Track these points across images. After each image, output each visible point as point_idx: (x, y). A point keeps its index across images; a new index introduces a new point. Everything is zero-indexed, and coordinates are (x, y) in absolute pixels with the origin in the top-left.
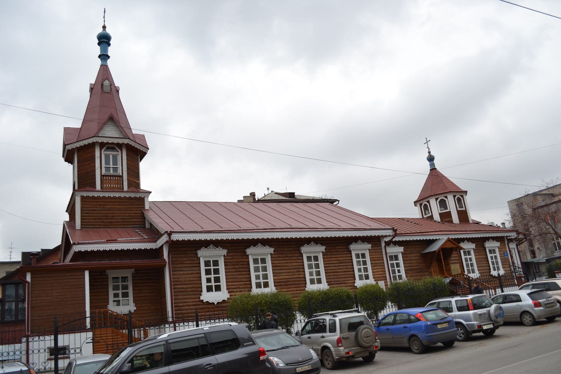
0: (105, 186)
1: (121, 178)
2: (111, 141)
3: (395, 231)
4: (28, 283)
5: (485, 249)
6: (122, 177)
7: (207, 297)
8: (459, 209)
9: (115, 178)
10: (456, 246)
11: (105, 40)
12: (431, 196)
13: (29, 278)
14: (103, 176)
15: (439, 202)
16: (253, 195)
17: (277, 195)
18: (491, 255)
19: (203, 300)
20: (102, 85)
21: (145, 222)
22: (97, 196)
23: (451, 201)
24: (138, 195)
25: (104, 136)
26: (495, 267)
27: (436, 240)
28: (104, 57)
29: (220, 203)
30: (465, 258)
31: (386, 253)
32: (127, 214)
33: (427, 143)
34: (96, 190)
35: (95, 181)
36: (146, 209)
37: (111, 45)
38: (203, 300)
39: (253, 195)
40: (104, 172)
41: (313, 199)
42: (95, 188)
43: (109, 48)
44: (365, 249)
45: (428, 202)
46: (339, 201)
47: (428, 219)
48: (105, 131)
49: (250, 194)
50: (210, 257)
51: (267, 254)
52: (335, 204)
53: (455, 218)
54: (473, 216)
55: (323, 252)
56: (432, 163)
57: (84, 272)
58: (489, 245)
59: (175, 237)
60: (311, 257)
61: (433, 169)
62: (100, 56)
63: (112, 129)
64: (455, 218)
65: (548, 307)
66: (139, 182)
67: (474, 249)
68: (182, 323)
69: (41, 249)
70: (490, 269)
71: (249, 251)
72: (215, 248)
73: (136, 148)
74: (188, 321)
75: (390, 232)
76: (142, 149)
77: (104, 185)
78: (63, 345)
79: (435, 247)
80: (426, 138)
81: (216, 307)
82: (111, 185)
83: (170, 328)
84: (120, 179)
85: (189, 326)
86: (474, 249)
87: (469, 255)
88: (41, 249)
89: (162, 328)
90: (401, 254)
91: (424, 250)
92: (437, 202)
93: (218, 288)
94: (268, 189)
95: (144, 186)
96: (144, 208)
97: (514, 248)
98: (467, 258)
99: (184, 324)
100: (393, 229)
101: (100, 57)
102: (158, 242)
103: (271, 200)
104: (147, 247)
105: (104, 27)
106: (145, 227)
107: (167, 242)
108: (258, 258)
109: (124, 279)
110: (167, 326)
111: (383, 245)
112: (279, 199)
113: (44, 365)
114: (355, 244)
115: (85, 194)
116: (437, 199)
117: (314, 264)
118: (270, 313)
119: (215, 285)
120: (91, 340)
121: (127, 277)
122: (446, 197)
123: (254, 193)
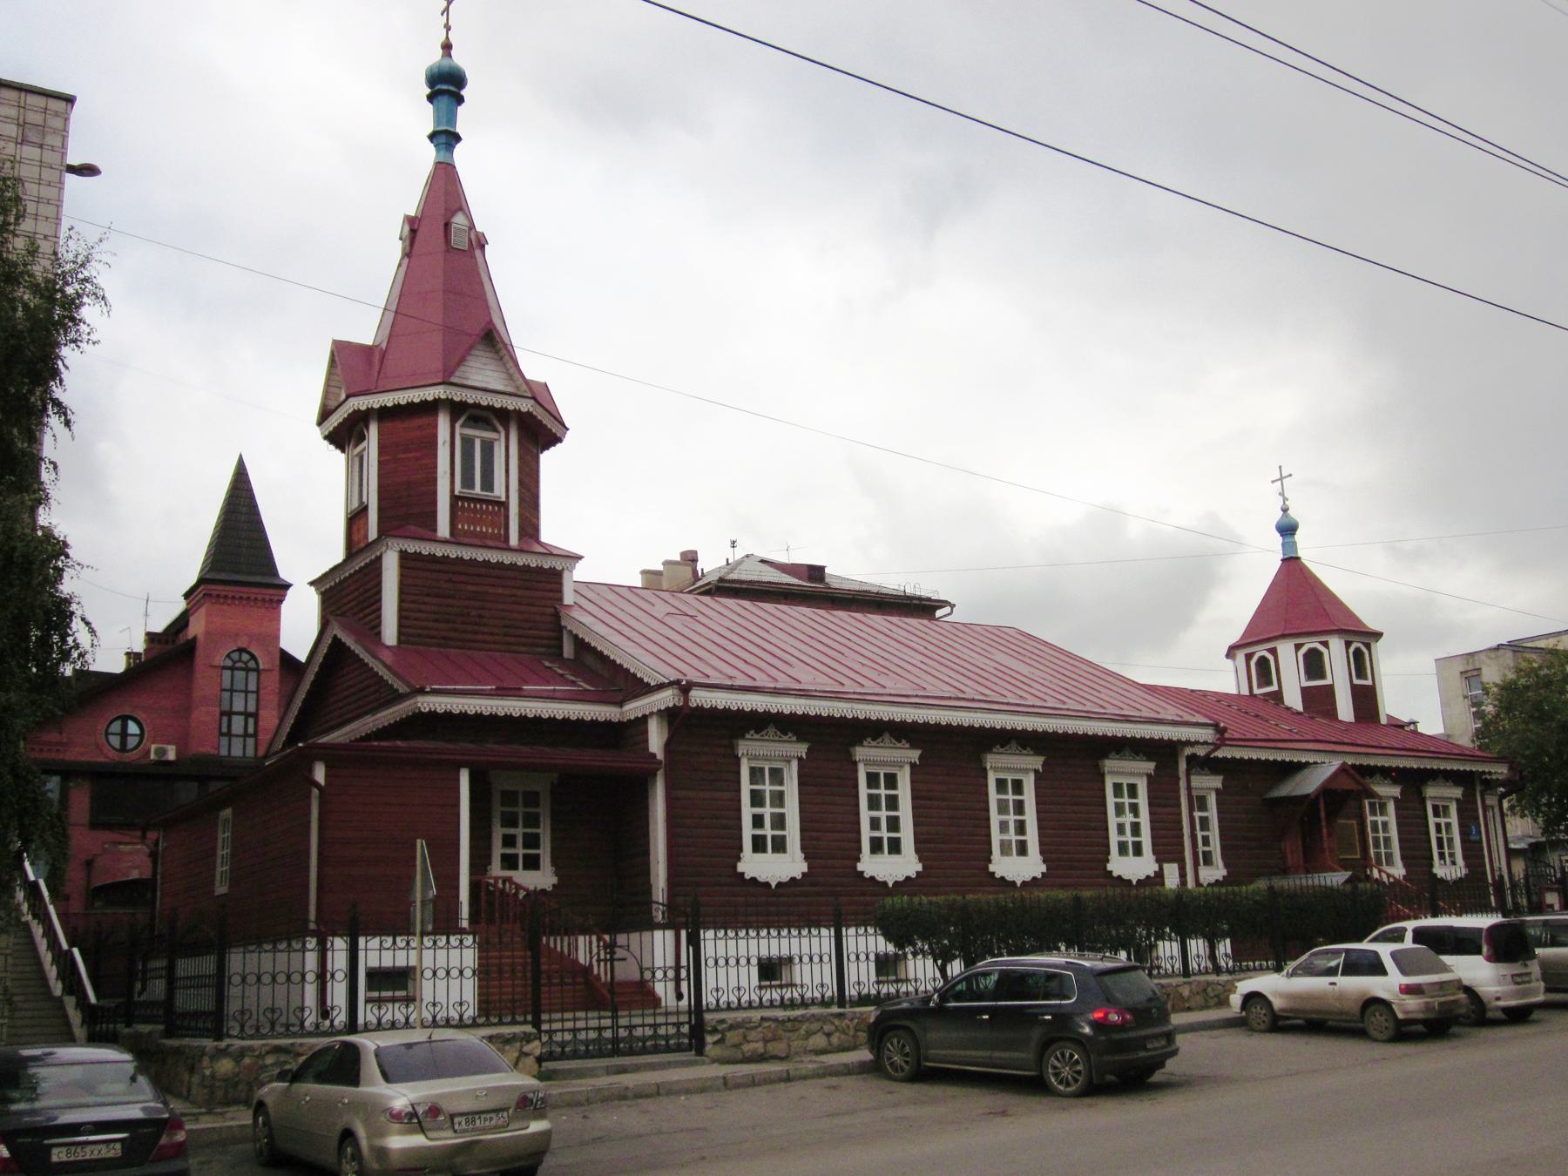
1: (502, 509)
2: (485, 400)
3: (1221, 731)
4: (317, 785)
5: (1423, 801)
6: (504, 505)
7: (754, 865)
8: (1356, 682)
10: (1360, 788)
11: (445, 87)
12: (1283, 636)
13: (320, 774)
15: (1306, 656)
16: (690, 558)
17: (765, 567)
18: (1438, 820)
20: (447, 225)
21: (560, 639)
22: (441, 554)
23: (1336, 655)
25: (465, 382)
27: (1307, 764)
28: (446, 138)
29: (611, 587)
30: (1116, 804)
31: (1189, 788)
32: (452, 606)
34: (436, 536)
35: (436, 511)
36: (565, 603)
39: (690, 558)
40: (458, 489)
41: (877, 593)
42: (435, 530)
43: (461, 109)
44: (1140, 775)
45: (1273, 651)
46: (952, 606)
47: (1267, 701)
48: (469, 369)
49: (684, 554)
50: (766, 758)
51: (900, 765)
52: (939, 613)
53: (1345, 709)
55: (1036, 771)
56: (1288, 539)
57: (459, 771)
59: (699, 698)
60: (877, 775)
61: (1291, 562)
62: (432, 137)
63: (485, 364)
64: (1345, 709)
65: (1518, 983)
67: (1396, 799)
70: (1431, 858)
71: (860, 753)
74: (818, 926)
75: (1207, 735)
76: (555, 429)
78: (391, 965)
79: (1310, 783)
80: (1280, 467)
81: (773, 896)
84: (499, 510)
86: (1396, 799)
91: (1271, 788)
93: (780, 845)
94: (733, 544)
96: (561, 599)
100: (1216, 726)
101: (432, 137)
102: (628, 707)
103: (759, 582)
105: (447, 47)
106: (561, 654)
109: (532, 799)
110: (454, 940)
111: (1183, 766)
113: (431, 1009)
115: (412, 547)
116: (1298, 647)
117: (1014, 800)
119: (889, 839)
122: (1325, 644)
123: (696, 552)
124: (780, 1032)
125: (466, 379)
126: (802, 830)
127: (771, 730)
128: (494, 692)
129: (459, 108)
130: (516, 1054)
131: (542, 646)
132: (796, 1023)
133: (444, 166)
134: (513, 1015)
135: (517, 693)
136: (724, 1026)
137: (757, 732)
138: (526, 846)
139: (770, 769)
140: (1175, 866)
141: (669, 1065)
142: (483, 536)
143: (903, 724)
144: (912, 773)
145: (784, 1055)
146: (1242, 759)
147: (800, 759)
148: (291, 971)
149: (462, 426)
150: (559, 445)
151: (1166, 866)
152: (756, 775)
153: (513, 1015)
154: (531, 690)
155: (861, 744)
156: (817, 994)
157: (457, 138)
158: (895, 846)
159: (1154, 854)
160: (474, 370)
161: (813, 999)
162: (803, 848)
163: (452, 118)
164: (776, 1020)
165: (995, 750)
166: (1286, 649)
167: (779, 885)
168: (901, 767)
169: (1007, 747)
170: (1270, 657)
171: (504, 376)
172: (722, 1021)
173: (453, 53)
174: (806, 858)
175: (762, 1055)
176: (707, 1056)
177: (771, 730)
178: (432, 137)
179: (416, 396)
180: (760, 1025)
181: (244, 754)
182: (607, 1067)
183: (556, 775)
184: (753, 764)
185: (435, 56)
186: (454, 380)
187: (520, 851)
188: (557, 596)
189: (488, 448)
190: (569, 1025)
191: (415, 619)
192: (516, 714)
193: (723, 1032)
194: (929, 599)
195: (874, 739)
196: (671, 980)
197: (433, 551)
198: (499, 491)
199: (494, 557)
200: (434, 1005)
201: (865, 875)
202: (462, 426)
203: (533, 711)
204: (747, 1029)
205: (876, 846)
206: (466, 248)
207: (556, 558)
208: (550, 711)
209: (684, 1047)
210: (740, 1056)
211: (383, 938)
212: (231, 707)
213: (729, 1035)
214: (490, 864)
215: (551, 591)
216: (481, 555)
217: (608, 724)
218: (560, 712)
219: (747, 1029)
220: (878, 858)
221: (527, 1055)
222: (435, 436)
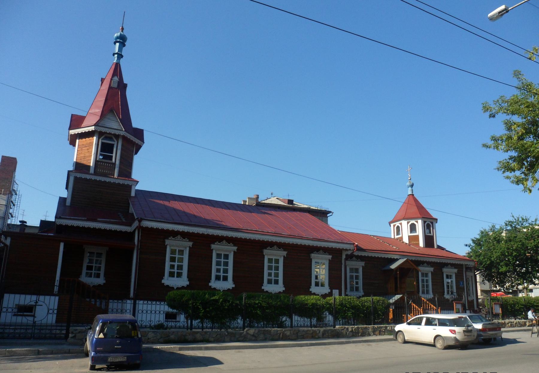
0: (98, 170)
5: (443, 273)
9: (109, 165)
14: (98, 161)
19: (164, 283)
24: (126, 182)
26: (424, 290)
33: (31, 301)
37: (126, 46)
38: (164, 283)
42: (89, 171)
43: (124, 48)
45: (401, 224)
54: (439, 241)
58: (446, 271)
66: (131, 171)
68: (146, 302)
69: (41, 220)
70: (444, 292)
72: (182, 239)
73: (132, 140)
77: (97, 170)
82: (104, 171)
83: (156, 305)
85: (127, 303)
87: (450, 278)
88: (41, 220)
89: (162, 305)
90: (455, 275)
92: (408, 225)
93: (225, 279)
95: (134, 176)
97: (472, 277)
98: (353, 275)
99: (148, 302)
104: (73, 224)
107: (137, 227)
108: (222, 254)
111: (344, 257)
112: (278, 204)
113: (149, 323)
114: (219, 244)
116: (408, 223)
118: (310, 307)
120: (35, 303)
121: (102, 254)
122: (417, 222)
123: (2, 156)
129: (123, 48)
137: (173, 237)
140: (338, 291)
144: (284, 260)
146: (371, 257)
148: (156, 310)
149: (102, 139)
151: (334, 290)
155: (168, 238)
157: (122, 56)
158: (276, 282)
159: (283, 284)
166: (404, 223)
168: (281, 257)
169: (273, 248)
170: (400, 226)
172: (76, 330)
174: (189, 280)
181: (172, 325)
184: (172, 248)
186: (100, 125)
194: (326, 211)
195: (317, 252)
196: (55, 314)
199: (108, 180)
201: (212, 287)
202: (102, 139)
220: (218, 282)
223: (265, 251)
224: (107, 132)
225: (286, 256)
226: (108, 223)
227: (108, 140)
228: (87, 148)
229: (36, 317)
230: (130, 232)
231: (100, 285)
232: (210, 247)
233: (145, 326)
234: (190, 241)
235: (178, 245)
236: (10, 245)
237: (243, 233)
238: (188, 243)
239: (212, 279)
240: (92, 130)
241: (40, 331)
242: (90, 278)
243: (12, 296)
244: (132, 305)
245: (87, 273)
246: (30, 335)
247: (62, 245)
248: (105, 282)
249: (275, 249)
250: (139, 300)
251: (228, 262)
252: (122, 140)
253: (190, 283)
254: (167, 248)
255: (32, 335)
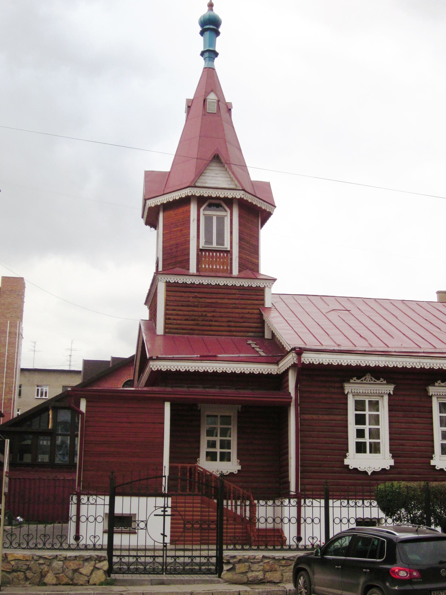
0: (203, 266)
2: (214, 194)
6: (229, 252)
11: (207, 27)
14: (202, 250)
20: (205, 101)
24: (254, 284)
34: (189, 272)
35: (189, 259)
42: (188, 269)
43: (218, 38)
59: (308, 358)
63: (217, 174)
72: (374, 381)
73: (255, 205)
76: (264, 206)
77: (202, 266)
84: (227, 255)
93: (375, 449)
96: (263, 305)
105: (211, 5)
106: (264, 336)
107: (294, 366)
120: (162, 511)
121: (230, 417)
124: (276, 566)
125: (206, 183)
126: (391, 439)
127: (368, 377)
128: (199, 359)
130: (92, 568)
131: (252, 332)
132: (289, 561)
133: (207, 69)
134: (266, 546)
135: (214, 359)
136: (235, 560)
137: (358, 378)
138: (221, 447)
139: (370, 402)
141: (194, 582)
142: (217, 270)
143: (386, 368)
145: (278, 581)
147: (389, 395)
148: (267, 517)
150: (272, 216)
152: (360, 405)
153: (266, 546)
154: (222, 357)
155: (348, 382)
156: (89, 542)
157: (216, 54)
160: (210, 178)
161: (86, 546)
162: (391, 451)
163: (212, 43)
164: (274, 558)
165: (352, 381)
167: (374, 473)
169: (363, 378)
171: (229, 179)
172: (234, 557)
173: (214, 8)
174: (393, 457)
175: (261, 580)
176: (222, 578)
177: (368, 377)
178: (202, 54)
179: (176, 196)
180: (262, 561)
182: (151, 580)
183: (240, 406)
185: (204, 11)
186: (198, 184)
187: (218, 450)
188: (262, 302)
189: (221, 220)
190: (204, 553)
191: (174, 319)
192: (201, 370)
193: (234, 564)
197: (185, 281)
198: (227, 246)
200: (313, 538)
201: (436, 468)
203: (221, 369)
204: (252, 563)
205: (360, 448)
206: (215, 112)
207: (260, 281)
208: (259, 370)
209: (140, 571)
210: (245, 580)
211: (342, 501)
212: (78, 372)
213: (237, 566)
214: (199, 457)
215: (257, 300)
216: (214, 281)
217: (270, 375)
218: (239, 369)
219: (252, 563)
221: (98, 569)
222: (189, 216)
223: (348, 388)
224: (213, 196)
225: (392, 393)
226: (261, 363)
227: (214, 211)
228: (179, 228)
229: (162, 534)
230: (277, 373)
231: (232, 474)
232: (427, 392)
233: (303, 547)
234: (388, 383)
235: (368, 393)
236: (86, 411)
237: (435, 359)
238: (385, 386)
239: (435, 453)
240: (186, 196)
241: (154, 559)
242: (213, 463)
243: (127, 499)
244: (323, 509)
245: (208, 454)
246: (160, 567)
247: (167, 407)
248: (239, 468)
249: (368, 382)
250: (333, 499)
251: (378, 416)
252: (238, 209)
253: (395, 463)
254: (349, 399)
255: (164, 567)
